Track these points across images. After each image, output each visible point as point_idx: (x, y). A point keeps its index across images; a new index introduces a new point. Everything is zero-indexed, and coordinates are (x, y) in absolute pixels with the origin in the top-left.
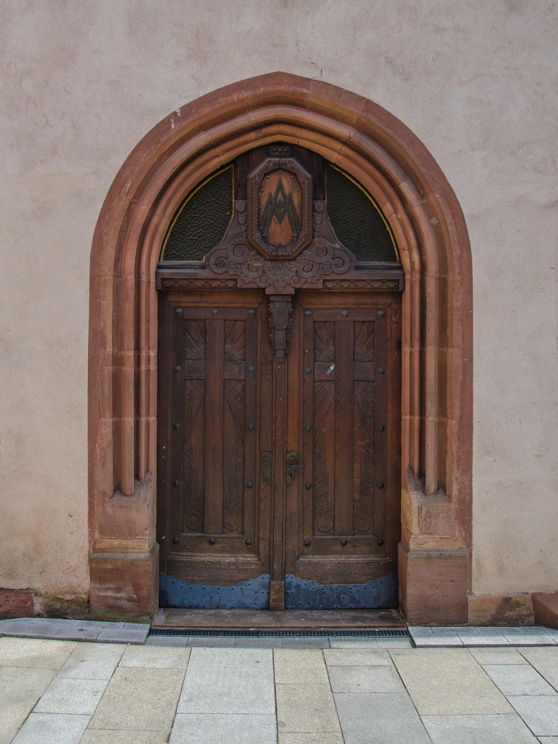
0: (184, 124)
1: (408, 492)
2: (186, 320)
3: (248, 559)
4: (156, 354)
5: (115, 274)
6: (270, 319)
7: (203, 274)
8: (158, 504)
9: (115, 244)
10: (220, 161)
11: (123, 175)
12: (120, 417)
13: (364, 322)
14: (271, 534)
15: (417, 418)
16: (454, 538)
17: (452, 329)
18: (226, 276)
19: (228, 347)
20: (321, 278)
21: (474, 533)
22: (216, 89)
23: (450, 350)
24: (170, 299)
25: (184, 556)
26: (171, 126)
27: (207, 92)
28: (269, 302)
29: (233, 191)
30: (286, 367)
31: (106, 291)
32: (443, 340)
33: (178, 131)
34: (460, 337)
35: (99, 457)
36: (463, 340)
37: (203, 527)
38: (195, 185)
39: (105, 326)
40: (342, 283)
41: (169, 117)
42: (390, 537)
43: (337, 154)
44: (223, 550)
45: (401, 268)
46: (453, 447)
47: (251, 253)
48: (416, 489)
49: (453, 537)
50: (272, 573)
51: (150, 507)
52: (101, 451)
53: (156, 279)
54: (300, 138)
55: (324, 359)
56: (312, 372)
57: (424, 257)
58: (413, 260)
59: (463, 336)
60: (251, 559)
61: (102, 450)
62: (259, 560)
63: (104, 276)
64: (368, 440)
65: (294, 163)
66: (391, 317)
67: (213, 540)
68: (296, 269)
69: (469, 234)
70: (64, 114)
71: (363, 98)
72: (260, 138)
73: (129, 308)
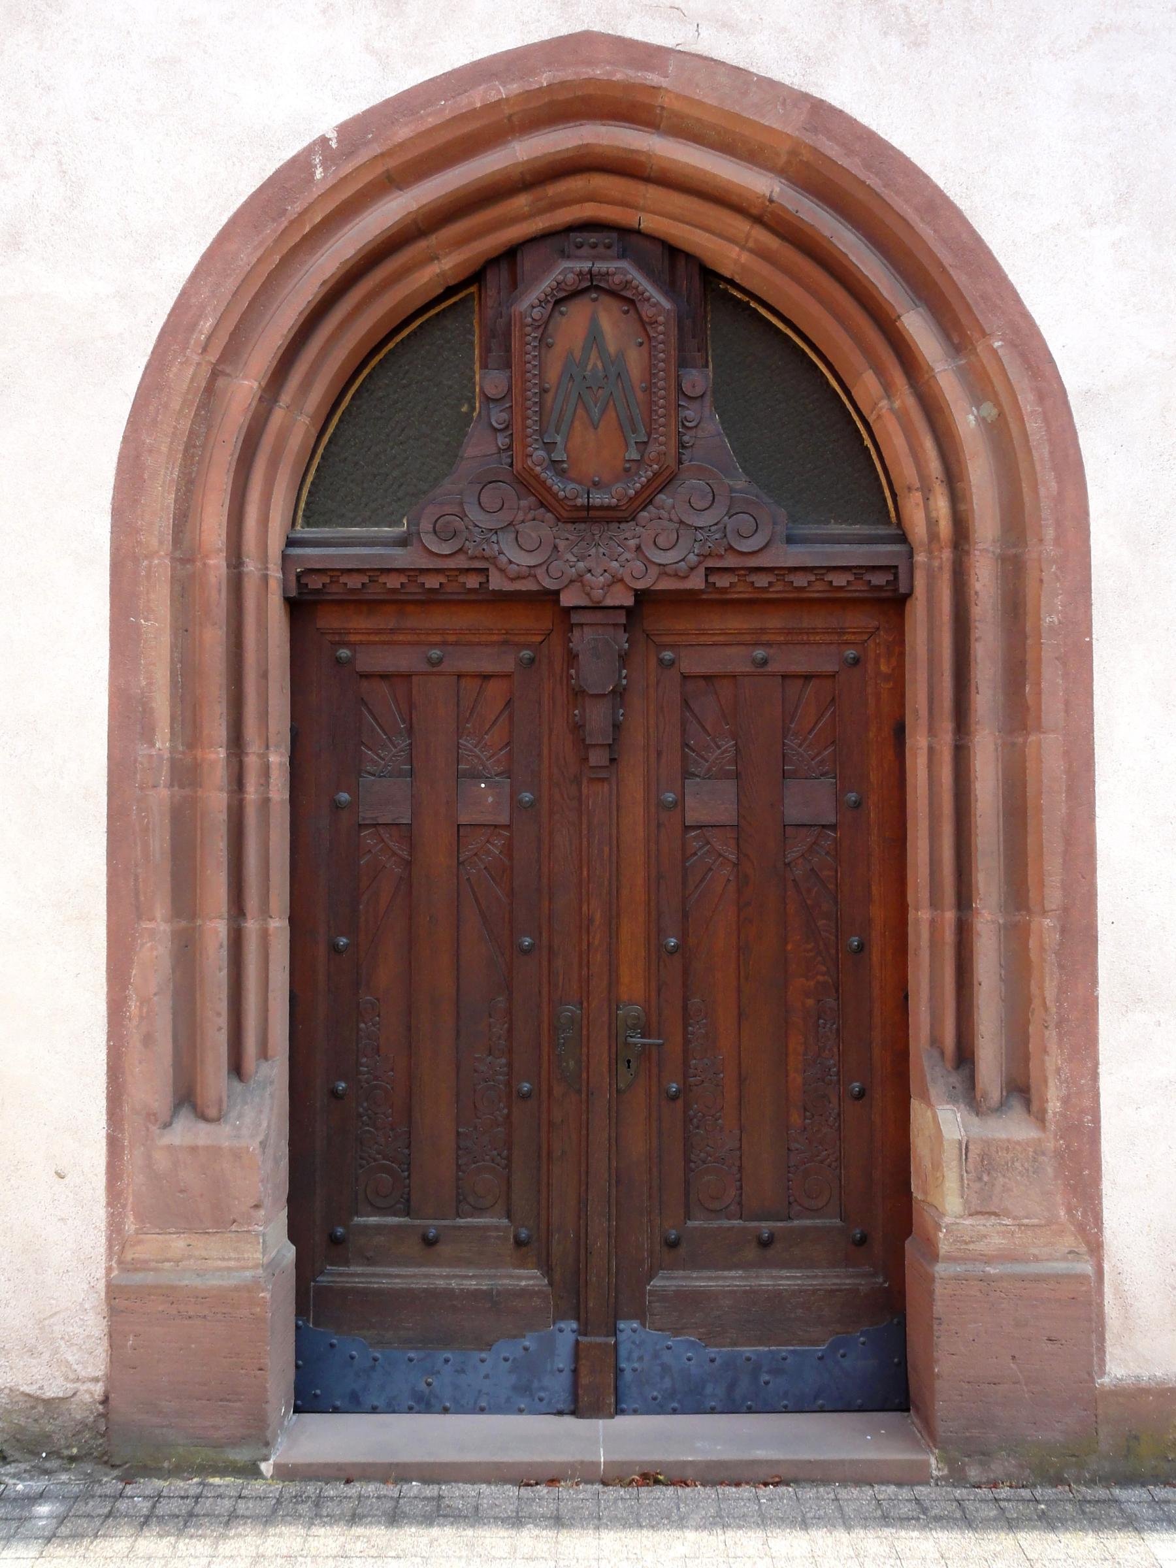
0: (348, 168)
1: (929, 1104)
2: (361, 676)
3: (523, 1283)
4: (286, 760)
5: (178, 554)
6: (573, 671)
7: (401, 557)
8: (292, 1144)
9: (175, 476)
10: (443, 274)
11: (193, 300)
12: (193, 916)
13: (807, 677)
14: (579, 1218)
15: (950, 915)
16: (1054, 1227)
17: (1039, 684)
18: (461, 562)
19: (467, 742)
20: (700, 563)
21: (1106, 1215)
22: (427, 78)
23: (1032, 738)
24: (321, 623)
25: (355, 1275)
26: (313, 174)
27: (406, 87)
28: (571, 627)
29: (477, 352)
30: (615, 792)
31: (153, 596)
32: (1019, 714)
33: (334, 188)
34: (1061, 706)
35: (135, 1022)
36: (1067, 711)
37: (408, 1200)
38: (382, 336)
39: (150, 684)
40: (753, 578)
41: (309, 151)
42: (881, 1221)
43: (737, 249)
44: (457, 1261)
45: (903, 538)
46: (1048, 985)
47: (523, 503)
48: (950, 1096)
49: (1049, 1223)
50: (583, 1315)
51: (270, 1151)
52: (142, 1004)
53: (284, 569)
54: (644, 209)
55: (709, 769)
56: (679, 804)
57: (962, 507)
58: (934, 514)
59: (1067, 703)
60: (531, 1282)
61: (143, 1001)
62: (551, 1284)
63: (146, 557)
64: (823, 975)
65: (624, 270)
66: (877, 663)
67: (432, 1233)
68: (636, 541)
69: (1081, 442)
70: (38, 143)
71: (806, 97)
72: (540, 212)
73: (214, 638)
